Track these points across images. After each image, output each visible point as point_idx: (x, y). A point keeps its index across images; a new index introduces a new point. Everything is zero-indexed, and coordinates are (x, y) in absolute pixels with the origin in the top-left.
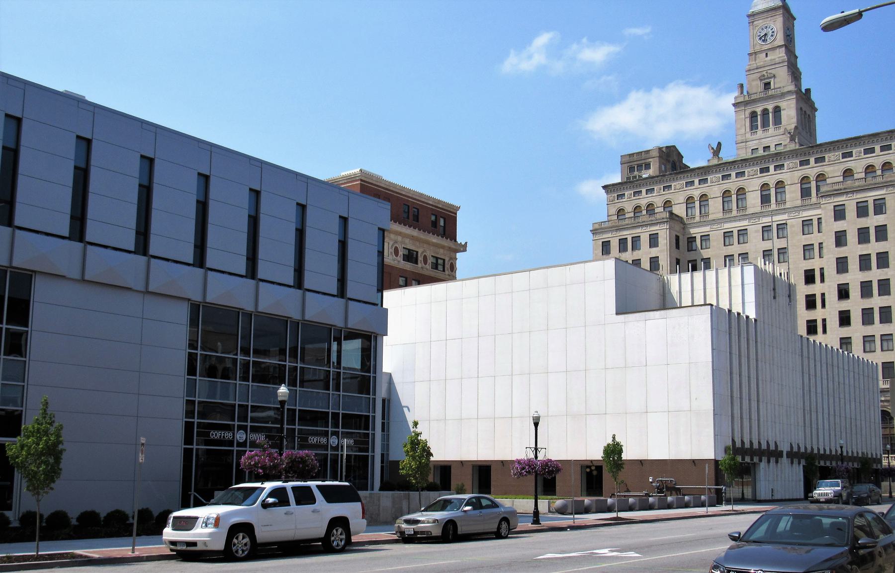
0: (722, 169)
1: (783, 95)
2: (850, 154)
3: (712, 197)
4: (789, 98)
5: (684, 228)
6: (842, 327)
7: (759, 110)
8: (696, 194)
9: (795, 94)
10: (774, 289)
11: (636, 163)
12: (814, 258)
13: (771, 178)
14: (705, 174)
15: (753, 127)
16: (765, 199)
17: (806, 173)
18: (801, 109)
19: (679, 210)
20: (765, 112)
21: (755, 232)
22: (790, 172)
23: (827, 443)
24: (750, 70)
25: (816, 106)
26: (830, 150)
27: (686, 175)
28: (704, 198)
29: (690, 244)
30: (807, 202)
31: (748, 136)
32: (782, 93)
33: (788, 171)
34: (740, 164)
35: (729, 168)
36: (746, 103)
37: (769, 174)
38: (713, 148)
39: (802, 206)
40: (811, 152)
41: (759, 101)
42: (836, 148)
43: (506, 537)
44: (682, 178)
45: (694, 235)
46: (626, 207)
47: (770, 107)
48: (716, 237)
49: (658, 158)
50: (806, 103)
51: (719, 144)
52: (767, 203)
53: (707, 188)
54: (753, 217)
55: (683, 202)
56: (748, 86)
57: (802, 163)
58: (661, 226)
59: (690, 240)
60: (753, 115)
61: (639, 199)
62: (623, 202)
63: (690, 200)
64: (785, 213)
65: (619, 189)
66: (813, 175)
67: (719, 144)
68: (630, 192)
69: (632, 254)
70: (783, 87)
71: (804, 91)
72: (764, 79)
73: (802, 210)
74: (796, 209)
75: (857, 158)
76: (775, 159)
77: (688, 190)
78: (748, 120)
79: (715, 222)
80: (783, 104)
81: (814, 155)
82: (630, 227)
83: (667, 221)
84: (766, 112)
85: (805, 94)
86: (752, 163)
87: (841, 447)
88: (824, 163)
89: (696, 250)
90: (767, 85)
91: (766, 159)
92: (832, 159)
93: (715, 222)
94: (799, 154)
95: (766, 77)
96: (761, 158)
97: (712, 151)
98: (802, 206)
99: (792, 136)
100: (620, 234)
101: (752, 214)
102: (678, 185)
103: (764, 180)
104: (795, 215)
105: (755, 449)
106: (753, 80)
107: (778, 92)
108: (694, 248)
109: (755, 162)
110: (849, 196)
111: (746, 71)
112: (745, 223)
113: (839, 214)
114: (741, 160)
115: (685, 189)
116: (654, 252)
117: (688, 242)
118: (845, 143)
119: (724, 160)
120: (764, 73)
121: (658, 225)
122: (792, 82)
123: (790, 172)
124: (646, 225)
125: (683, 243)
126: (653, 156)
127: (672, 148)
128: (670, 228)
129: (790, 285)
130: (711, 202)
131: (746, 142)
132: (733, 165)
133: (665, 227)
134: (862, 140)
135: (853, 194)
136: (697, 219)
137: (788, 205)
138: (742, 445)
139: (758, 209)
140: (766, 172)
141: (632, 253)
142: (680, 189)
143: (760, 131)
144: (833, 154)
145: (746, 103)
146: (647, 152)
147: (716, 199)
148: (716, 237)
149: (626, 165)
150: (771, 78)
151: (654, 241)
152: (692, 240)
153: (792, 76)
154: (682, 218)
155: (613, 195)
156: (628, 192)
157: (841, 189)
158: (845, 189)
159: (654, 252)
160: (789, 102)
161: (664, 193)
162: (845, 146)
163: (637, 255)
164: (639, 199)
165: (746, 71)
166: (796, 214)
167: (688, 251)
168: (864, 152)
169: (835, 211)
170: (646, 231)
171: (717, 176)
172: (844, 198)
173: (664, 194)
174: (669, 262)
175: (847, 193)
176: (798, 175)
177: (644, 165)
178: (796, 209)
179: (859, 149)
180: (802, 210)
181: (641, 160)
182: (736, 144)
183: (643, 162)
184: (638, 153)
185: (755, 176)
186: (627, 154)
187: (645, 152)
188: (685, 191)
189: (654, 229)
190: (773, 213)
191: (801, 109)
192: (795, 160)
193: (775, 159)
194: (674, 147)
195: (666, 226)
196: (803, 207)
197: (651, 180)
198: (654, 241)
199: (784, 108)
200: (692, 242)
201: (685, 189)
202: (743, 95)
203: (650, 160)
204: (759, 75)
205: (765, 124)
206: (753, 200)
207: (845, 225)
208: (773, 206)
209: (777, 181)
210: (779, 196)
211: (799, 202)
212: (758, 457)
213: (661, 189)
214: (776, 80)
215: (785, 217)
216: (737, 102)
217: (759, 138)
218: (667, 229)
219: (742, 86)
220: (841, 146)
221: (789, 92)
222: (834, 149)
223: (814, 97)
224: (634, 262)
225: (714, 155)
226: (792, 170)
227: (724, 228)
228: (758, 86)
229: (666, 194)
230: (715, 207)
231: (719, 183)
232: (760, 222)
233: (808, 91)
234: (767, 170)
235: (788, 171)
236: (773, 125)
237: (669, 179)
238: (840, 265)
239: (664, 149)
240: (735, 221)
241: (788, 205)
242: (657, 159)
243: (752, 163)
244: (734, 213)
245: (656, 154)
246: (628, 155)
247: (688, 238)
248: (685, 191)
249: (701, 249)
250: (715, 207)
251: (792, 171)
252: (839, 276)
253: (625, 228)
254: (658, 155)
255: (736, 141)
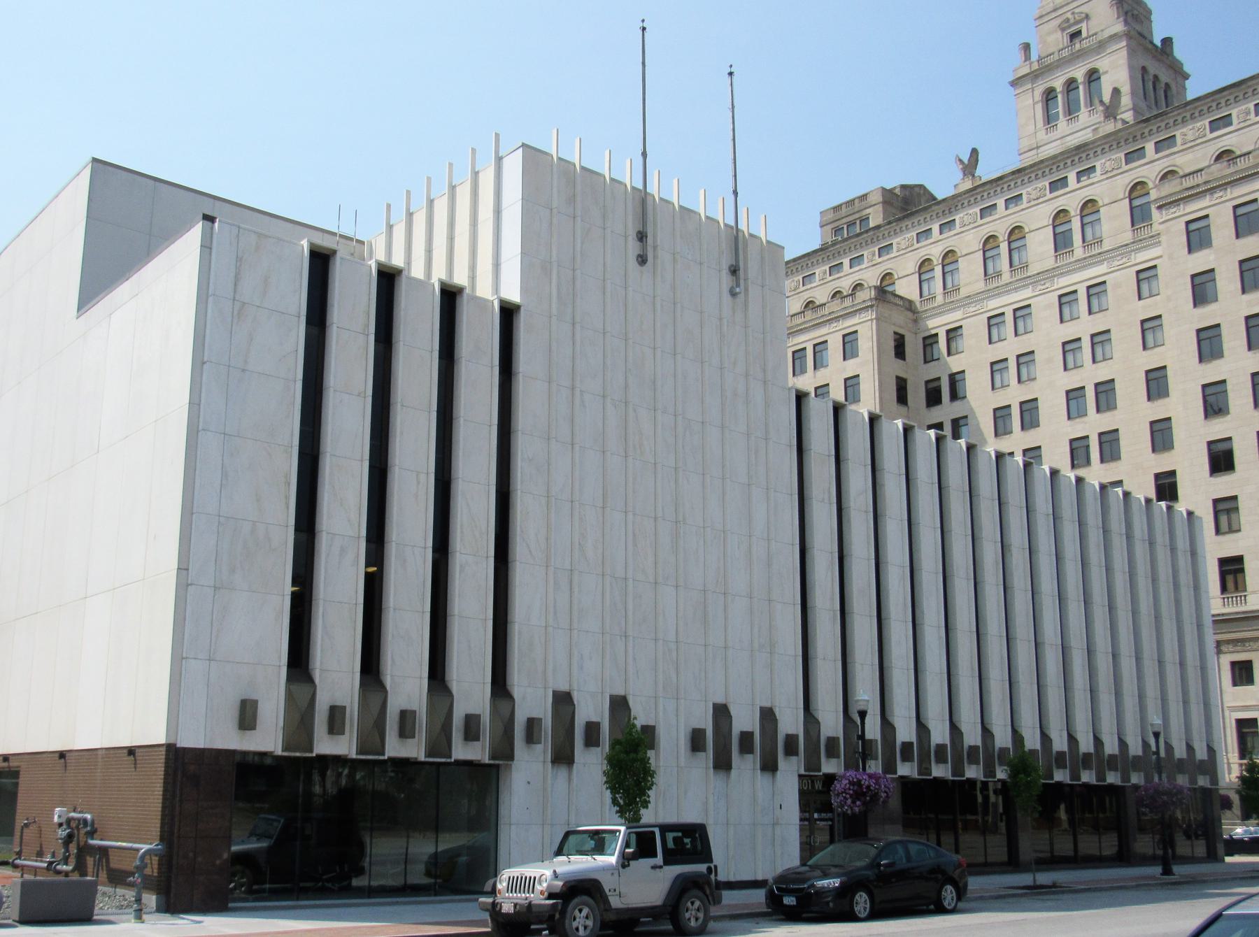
0: (979, 197)
1: (1101, 46)
2: (1226, 121)
3: (963, 254)
4: (1115, 48)
5: (915, 321)
6: (1216, 477)
7: (1058, 84)
8: (935, 251)
9: (1124, 38)
10: (642, 236)
11: (844, 221)
12: (1163, 345)
13: (1071, 200)
14: (950, 212)
15: (1049, 119)
16: (1061, 242)
17: (1140, 174)
18: (1144, 69)
19: (906, 288)
20: (1071, 85)
21: (1044, 306)
22: (1107, 178)
23: (866, 693)
24: (1041, 17)
25: (1187, 68)
26: (1184, 121)
27: (916, 221)
28: (949, 257)
29: (928, 349)
30: (1145, 233)
31: (1042, 136)
32: (1100, 42)
33: (1105, 177)
34: (1011, 180)
35: (992, 192)
36: (1034, 76)
37: (1067, 190)
38: (960, 161)
39: (1133, 243)
40: (1146, 131)
41: (1057, 67)
42: (1197, 114)
43: (953, 911)
44: (910, 226)
45: (933, 332)
46: (818, 297)
47: (1079, 73)
48: (974, 329)
49: (881, 205)
50: (1159, 60)
51: (974, 152)
52: (1065, 247)
53: (956, 237)
54: (1041, 280)
55: (913, 271)
56: (1040, 46)
57: (1130, 158)
58: (863, 315)
59: (928, 342)
60: (1049, 95)
61: (838, 278)
62: (812, 288)
63: (924, 266)
64: (1101, 262)
65: (805, 266)
66: (1153, 176)
67: (974, 152)
68: (824, 268)
69: (815, 377)
70: (1102, 30)
71: (1158, 44)
72: (1069, 27)
73: (1134, 250)
74: (1123, 249)
75: (1242, 125)
76: (1076, 159)
77: (921, 247)
78: (1039, 108)
79: (971, 299)
80: (1102, 63)
81: (1153, 136)
82: (810, 327)
83: (872, 306)
84: (1073, 86)
85: (1162, 49)
86: (1033, 175)
87: (1156, 735)
88: (1175, 149)
89: (938, 359)
90: (1075, 35)
91: (1059, 161)
92: (1190, 137)
93: (971, 299)
94: (1122, 141)
95: (1072, 21)
96: (1050, 162)
97: (961, 166)
98: (1133, 243)
99: (1107, 108)
100: (793, 343)
101: (1038, 274)
102: (903, 241)
103: (1059, 204)
104: (1121, 262)
105: (1134, 757)
106: (1049, 34)
107: (1093, 40)
108: (935, 357)
109: (1040, 173)
110: (1216, 195)
111: (1035, 20)
112: (1027, 293)
113: (1197, 236)
114: (1013, 173)
115: (916, 246)
116: (851, 367)
117: (925, 347)
118: (1213, 101)
119: (984, 179)
120: (1069, 15)
121: (858, 315)
122: (1118, 18)
123: (1107, 178)
124: (837, 319)
125: (913, 347)
126: (874, 203)
127: (917, 189)
128: (877, 319)
129: (642, 199)
130: (962, 263)
131: (1038, 148)
132: (998, 186)
133: (869, 318)
134: (1249, 87)
135: (1226, 189)
136: (940, 299)
137: (1106, 246)
138: (1043, 744)
139: (1049, 263)
140: (1062, 188)
141: (815, 373)
142: (906, 248)
143: (1062, 124)
144: (1190, 127)
145: (1034, 76)
146: (863, 197)
147: (971, 256)
148: (974, 329)
149: (830, 227)
150: (1080, 21)
151: (849, 345)
152: (929, 341)
153: (1117, 8)
154: (910, 302)
155: (796, 279)
156: (820, 269)
157: (1198, 185)
158: (1205, 183)
159: (851, 367)
160: (1114, 57)
161: (880, 260)
162: (1214, 105)
163: (822, 377)
164: (838, 278)
165: (1035, 20)
166: (1124, 260)
167: (926, 362)
168: (1255, 110)
169: (1188, 233)
170: (837, 328)
171: (971, 212)
172: (1206, 201)
173: (880, 263)
174: (877, 384)
175: (1211, 191)
176: (1122, 183)
177: (858, 222)
178: (1123, 249)
179: (1244, 107)
180: (1134, 250)
181: (854, 213)
182: (1020, 155)
183: (857, 216)
184: (848, 202)
185: (1041, 200)
186: (829, 207)
187: (859, 198)
188: (915, 250)
189: (848, 324)
190: (1084, 263)
191: (1144, 69)
192: (1116, 153)
193: (1076, 159)
194: (921, 186)
195: (870, 315)
196: (1138, 244)
197: (856, 239)
198: (849, 345)
199: (1105, 70)
200: (931, 345)
201: (916, 246)
202: (1028, 62)
203: (868, 211)
204: (1059, 21)
205: (1071, 110)
206: (1040, 246)
207: (1212, 257)
208: (1079, 252)
209: (1083, 201)
210: (1088, 230)
211: (1128, 236)
212: (1208, 776)
213: (874, 255)
214: (1090, 22)
215: (1102, 269)
216: (1017, 77)
217: (1060, 136)
218: (872, 320)
219: (1027, 47)
220: (1205, 108)
221: (1114, 38)
222: (1193, 117)
223: (1178, 52)
224: (819, 392)
225: (965, 175)
226: (1109, 174)
227: (989, 308)
228: (1057, 40)
229: (884, 261)
230: (970, 272)
231: (976, 224)
232: (1053, 288)
233: (1167, 42)
234: (1063, 182)
235: (1105, 177)
236: (1086, 106)
237: (886, 233)
238: (1205, 344)
239: (897, 191)
240: (1008, 292)
241: (1106, 246)
242: (880, 208)
243: (1033, 175)
244: (1006, 277)
245: (877, 198)
246: (831, 208)
247: (925, 339)
248: (915, 250)
249: (949, 354)
250: (970, 272)
251: (1111, 177)
252: (1204, 366)
253: (801, 330)
254: (881, 199)
255: (1019, 150)
